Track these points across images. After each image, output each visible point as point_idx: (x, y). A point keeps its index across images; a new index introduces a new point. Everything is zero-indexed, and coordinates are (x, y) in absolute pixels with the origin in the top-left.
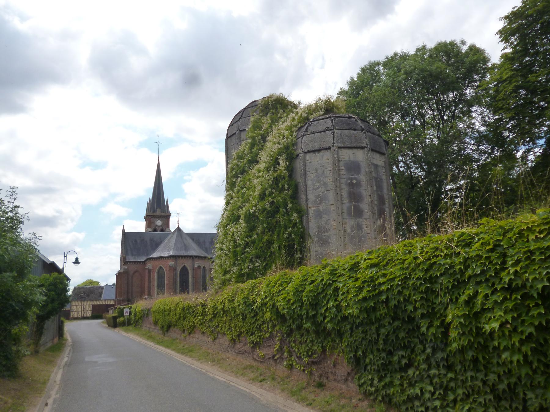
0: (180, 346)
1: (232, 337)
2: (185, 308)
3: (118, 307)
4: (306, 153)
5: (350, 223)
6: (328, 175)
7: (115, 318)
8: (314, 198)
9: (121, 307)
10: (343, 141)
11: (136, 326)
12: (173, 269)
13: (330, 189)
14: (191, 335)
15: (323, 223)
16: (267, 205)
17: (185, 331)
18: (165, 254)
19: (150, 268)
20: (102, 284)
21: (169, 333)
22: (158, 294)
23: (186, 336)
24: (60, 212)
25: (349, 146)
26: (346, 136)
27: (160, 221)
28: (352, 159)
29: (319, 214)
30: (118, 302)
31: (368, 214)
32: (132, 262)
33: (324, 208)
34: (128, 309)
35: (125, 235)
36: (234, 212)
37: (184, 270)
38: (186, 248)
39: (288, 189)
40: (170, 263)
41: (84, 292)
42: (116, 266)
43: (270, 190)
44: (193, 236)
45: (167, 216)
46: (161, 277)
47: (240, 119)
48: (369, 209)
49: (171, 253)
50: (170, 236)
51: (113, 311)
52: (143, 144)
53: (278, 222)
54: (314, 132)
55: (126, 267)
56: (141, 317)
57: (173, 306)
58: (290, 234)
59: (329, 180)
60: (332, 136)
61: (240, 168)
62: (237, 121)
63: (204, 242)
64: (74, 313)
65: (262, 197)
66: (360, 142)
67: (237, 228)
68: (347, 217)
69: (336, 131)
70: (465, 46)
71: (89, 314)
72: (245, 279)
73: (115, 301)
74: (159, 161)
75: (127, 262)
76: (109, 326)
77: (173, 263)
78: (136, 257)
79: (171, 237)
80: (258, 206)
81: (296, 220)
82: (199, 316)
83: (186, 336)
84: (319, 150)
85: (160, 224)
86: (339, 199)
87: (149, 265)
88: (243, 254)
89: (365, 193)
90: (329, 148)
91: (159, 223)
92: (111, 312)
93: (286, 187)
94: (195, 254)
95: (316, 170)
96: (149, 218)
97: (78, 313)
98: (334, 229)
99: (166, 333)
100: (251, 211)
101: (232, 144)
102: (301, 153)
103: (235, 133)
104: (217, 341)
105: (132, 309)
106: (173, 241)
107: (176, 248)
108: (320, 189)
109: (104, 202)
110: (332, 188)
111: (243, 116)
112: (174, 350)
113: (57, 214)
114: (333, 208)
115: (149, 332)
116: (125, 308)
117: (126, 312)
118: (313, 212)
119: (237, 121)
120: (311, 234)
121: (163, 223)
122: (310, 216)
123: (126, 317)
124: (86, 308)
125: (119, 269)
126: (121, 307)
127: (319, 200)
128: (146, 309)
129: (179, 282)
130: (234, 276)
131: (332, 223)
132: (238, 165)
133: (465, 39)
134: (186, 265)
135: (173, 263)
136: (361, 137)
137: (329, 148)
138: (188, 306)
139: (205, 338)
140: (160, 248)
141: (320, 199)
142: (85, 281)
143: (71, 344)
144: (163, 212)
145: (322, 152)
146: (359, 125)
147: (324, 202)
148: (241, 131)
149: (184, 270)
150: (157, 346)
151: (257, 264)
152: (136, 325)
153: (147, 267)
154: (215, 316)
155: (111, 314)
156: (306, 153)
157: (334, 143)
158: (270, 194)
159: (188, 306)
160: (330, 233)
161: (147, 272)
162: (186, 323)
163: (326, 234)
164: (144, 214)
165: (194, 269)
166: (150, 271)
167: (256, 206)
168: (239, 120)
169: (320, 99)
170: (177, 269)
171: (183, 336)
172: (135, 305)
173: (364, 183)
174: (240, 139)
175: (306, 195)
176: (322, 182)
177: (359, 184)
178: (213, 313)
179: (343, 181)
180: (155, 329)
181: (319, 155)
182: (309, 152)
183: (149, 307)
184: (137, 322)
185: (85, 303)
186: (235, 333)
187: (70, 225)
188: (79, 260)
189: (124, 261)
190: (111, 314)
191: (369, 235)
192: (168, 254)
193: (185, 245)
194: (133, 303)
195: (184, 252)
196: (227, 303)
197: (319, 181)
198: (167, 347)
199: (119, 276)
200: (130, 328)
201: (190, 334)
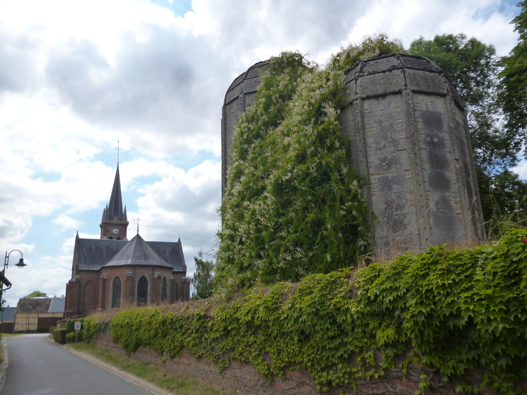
0: (160, 375)
1: (269, 369)
2: (166, 321)
3: (68, 320)
4: (363, 99)
5: (434, 197)
6: (399, 129)
7: (64, 333)
8: (378, 162)
9: (72, 320)
10: (417, 83)
11: (88, 342)
12: (130, 279)
13: (402, 149)
14: (176, 360)
15: (393, 196)
16: (313, 168)
17: (164, 353)
18: (123, 262)
19: (106, 277)
20: (50, 296)
21: (137, 354)
22: (113, 307)
23: (166, 361)
24: (10, 223)
25: (427, 90)
26: (421, 78)
27: (116, 230)
28: (430, 109)
29: (387, 184)
30: (67, 314)
31: (457, 186)
32: (86, 271)
33: (395, 175)
34: (80, 323)
35: (79, 242)
36: (251, 185)
37: (143, 281)
38: (146, 256)
39: (341, 147)
40: (128, 272)
41: (30, 304)
42: (67, 276)
43: (313, 148)
44: (153, 245)
45: (124, 225)
46: (117, 288)
47: (244, 80)
48: (457, 179)
49: (129, 262)
50: (127, 245)
51: (61, 324)
52: (98, 158)
53: (331, 191)
54: (374, 73)
55: (78, 277)
56: (95, 333)
57: (146, 319)
58: (349, 212)
59: (401, 136)
60: (402, 75)
61: (252, 132)
62: (239, 84)
63: (164, 252)
64: (18, 327)
65: (301, 158)
66: (440, 88)
67: (260, 205)
68: (429, 189)
69: (407, 70)
70: (464, 40)
71: (35, 327)
72: (278, 276)
73: (64, 314)
74: (118, 167)
75: (80, 271)
76: (56, 341)
77: (131, 272)
78: (90, 266)
79: (129, 245)
80: (295, 171)
81: (356, 191)
82: (192, 332)
83: (166, 361)
84: (383, 96)
85: (117, 233)
86: (418, 161)
87: (104, 275)
88: (273, 240)
89: (450, 157)
90: (400, 92)
91: (115, 231)
92: (59, 325)
93: (337, 144)
94: (156, 263)
95: (380, 122)
96: (105, 227)
97: (22, 326)
98: (411, 205)
99: (132, 353)
100: (284, 178)
101: (232, 111)
102: (356, 100)
103: (238, 97)
104: (229, 373)
105: (84, 323)
106: (132, 248)
107: (135, 257)
108: (387, 149)
109: (56, 214)
110: (406, 147)
111: (248, 77)
112: (152, 381)
113: (6, 225)
114: (408, 175)
115: (107, 351)
116: (76, 321)
117: (77, 326)
118: (377, 181)
119: (239, 84)
120: (376, 213)
121: (119, 232)
122: (372, 186)
123: (77, 332)
124: (32, 321)
125: (71, 278)
126: (72, 320)
127: (386, 164)
128: (103, 323)
129: (136, 293)
130: (260, 272)
131: (409, 197)
132: (249, 129)
133: (465, 33)
134: (145, 275)
135: (131, 272)
136: (440, 81)
137: (400, 92)
138: (172, 319)
139: (203, 366)
140: (117, 256)
141: (387, 162)
142: (31, 292)
143: (7, 366)
144: (120, 220)
145: (388, 97)
146: (434, 67)
147: (394, 166)
148: (245, 94)
149: (143, 281)
150: (124, 373)
151: (299, 255)
152: (88, 341)
153: (102, 277)
154: (227, 332)
155: (59, 328)
156: (363, 99)
157: (406, 85)
158: (314, 154)
159: (172, 319)
160: (406, 210)
161: (101, 282)
162: (166, 342)
163: (399, 212)
164: (100, 222)
165: (154, 280)
166: (105, 281)
167: (291, 171)
168: (242, 82)
169: (369, 39)
170: (136, 279)
171: (159, 360)
172: (88, 317)
173: (448, 142)
174: (244, 104)
175: (366, 157)
176: (390, 140)
177: (441, 144)
178: (225, 328)
179: (422, 137)
180: (115, 347)
181: (383, 102)
182: (368, 98)
183: (108, 320)
184: (90, 338)
185: (31, 315)
186: (274, 362)
187: (19, 237)
188: (25, 262)
189: (76, 269)
190: (59, 328)
191: (460, 216)
192: (126, 262)
193: (144, 253)
194: (85, 315)
195: (143, 261)
196: (261, 312)
197: (385, 138)
198: (140, 375)
199: (70, 286)
200: (82, 344)
201: (173, 357)
